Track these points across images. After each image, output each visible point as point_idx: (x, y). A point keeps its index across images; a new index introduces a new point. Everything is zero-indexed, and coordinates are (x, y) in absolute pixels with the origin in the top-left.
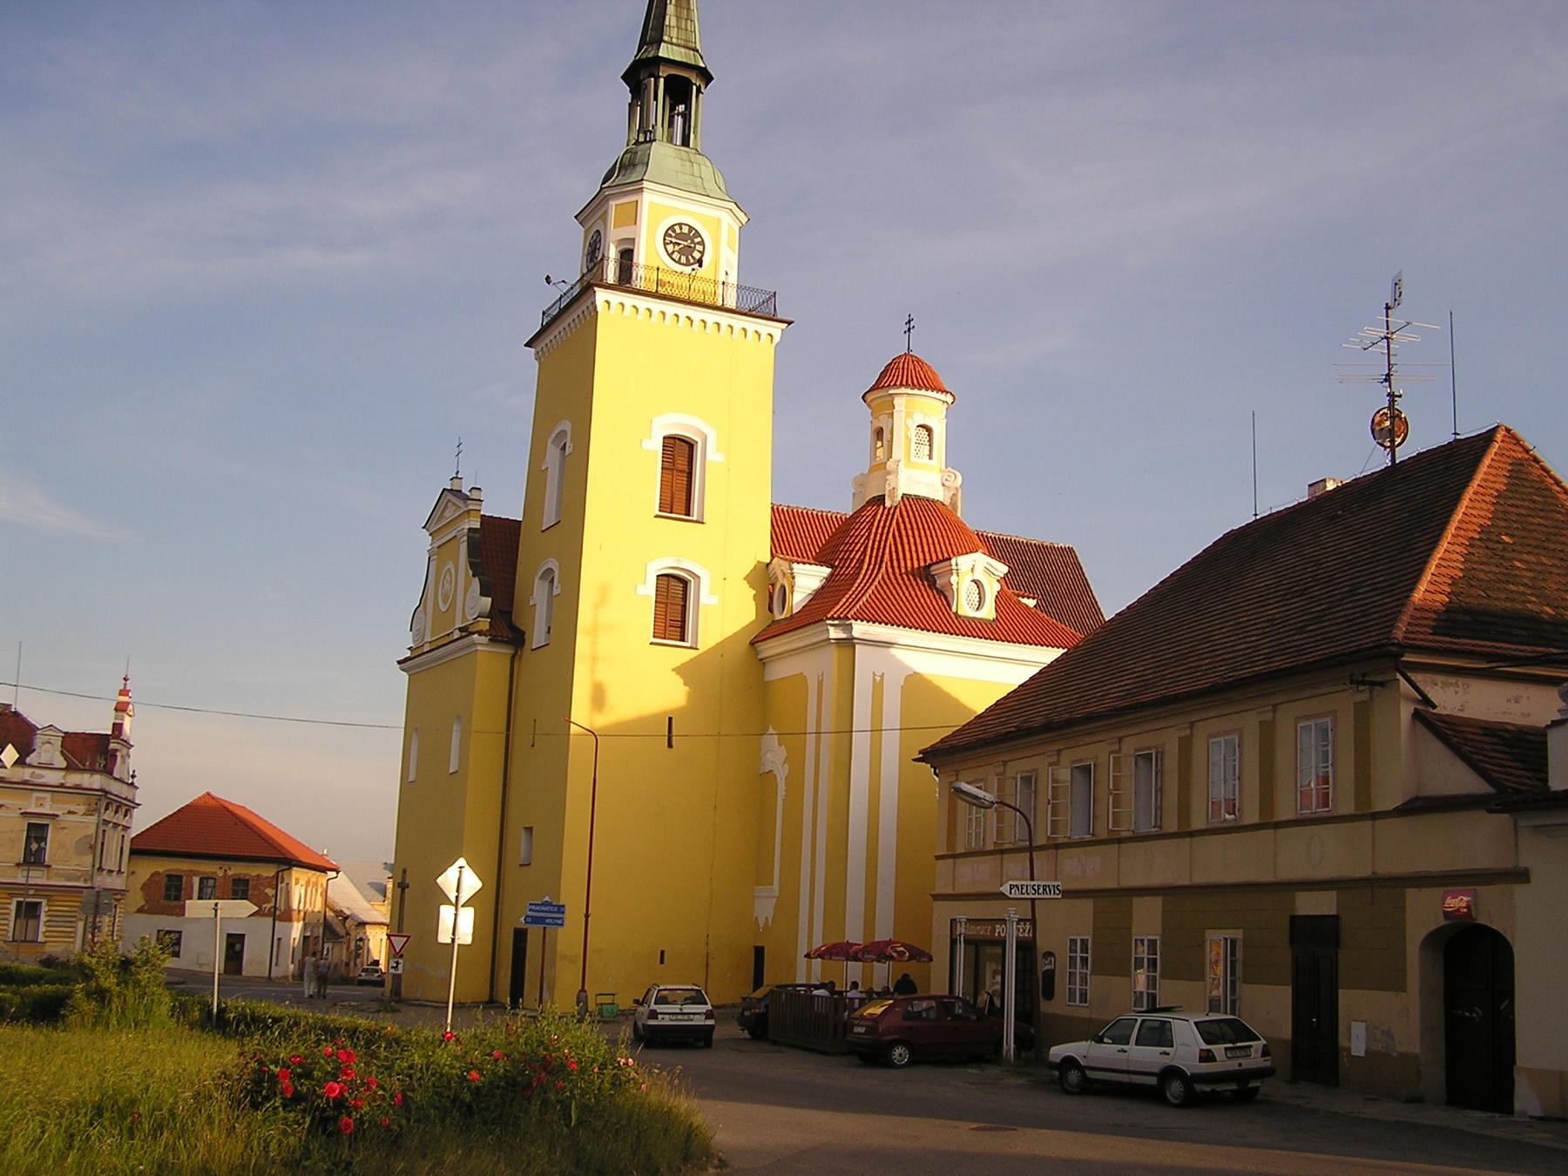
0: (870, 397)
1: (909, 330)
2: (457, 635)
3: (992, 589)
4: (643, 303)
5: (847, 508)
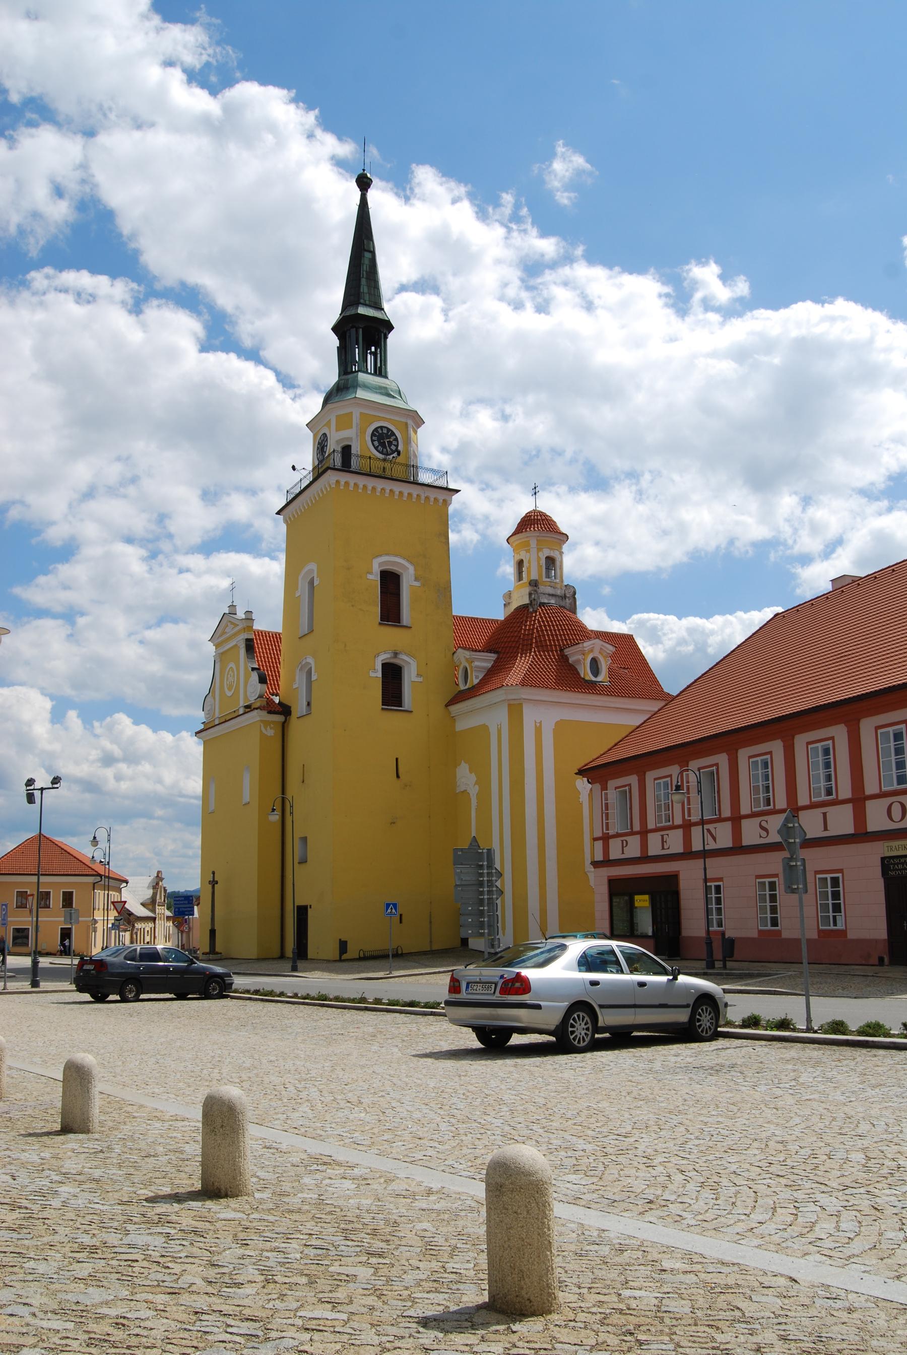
0: (511, 540)
1: (535, 493)
2: (241, 712)
4: (362, 481)
5: (500, 614)
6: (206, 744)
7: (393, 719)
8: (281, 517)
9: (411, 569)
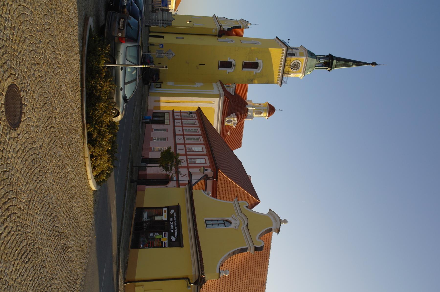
2: (220, 24)
3: (230, 124)
6: (212, 17)
7: (216, 64)
8: (275, 38)
9: (259, 72)
